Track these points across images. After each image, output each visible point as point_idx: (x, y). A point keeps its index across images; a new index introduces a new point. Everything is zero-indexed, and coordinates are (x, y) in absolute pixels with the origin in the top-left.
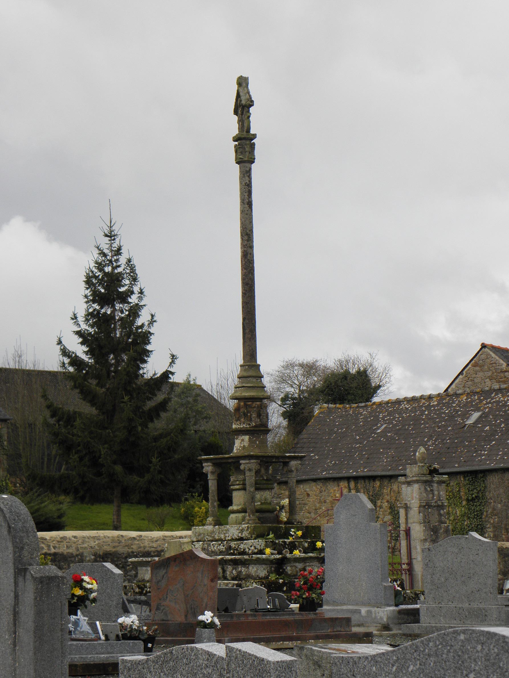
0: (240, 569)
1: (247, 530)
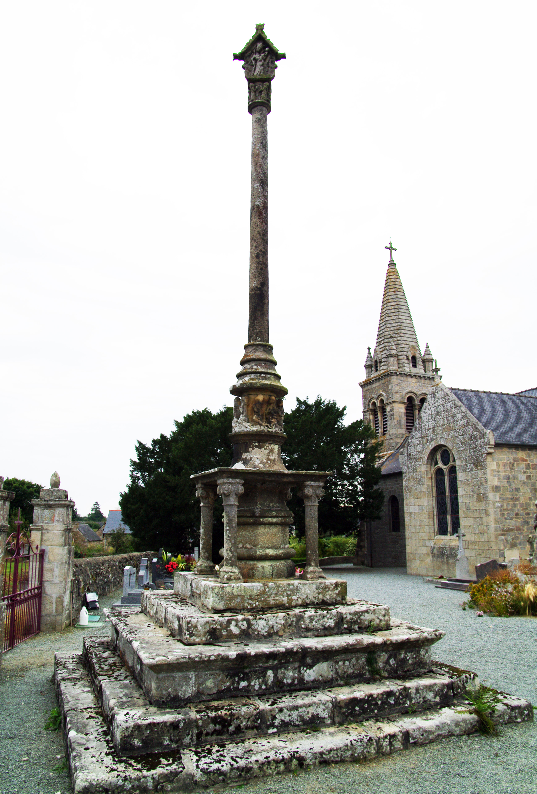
0: (402, 656)
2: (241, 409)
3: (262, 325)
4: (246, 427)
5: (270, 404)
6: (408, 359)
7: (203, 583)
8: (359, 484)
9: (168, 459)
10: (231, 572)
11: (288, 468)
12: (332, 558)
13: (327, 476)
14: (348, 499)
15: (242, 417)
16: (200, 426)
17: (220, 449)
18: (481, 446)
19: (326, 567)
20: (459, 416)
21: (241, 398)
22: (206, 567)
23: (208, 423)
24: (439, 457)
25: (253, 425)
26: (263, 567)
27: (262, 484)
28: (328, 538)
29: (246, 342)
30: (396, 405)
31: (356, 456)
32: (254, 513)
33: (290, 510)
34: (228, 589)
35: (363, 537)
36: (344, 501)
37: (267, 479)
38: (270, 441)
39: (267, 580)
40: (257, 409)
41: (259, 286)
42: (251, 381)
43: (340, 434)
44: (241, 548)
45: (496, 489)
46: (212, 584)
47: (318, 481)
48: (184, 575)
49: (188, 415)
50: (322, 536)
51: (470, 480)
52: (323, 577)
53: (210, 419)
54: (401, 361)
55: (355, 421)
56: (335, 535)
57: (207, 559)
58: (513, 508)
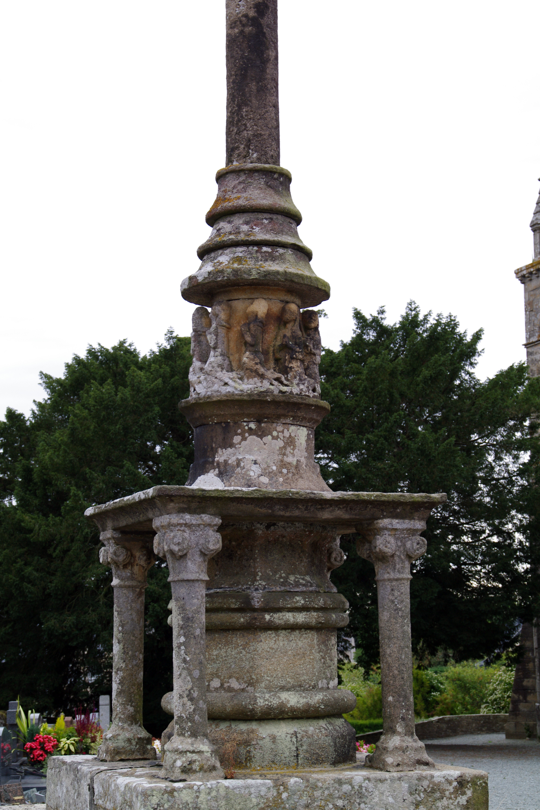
2: (211, 338)
3: (262, 117)
4: (226, 384)
5: (285, 323)
7: (122, 781)
8: (518, 530)
9: (28, 472)
10: (193, 752)
11: (334, 488)
12: (450, 720)
13: (433, 504)
14: (489, 567)
15: (214, 358)
16: (108, 387)
17: (161, 444)
19: (436, 742)
21: (209, 310)
22: (129, 740)
23: (128, 379)
25: (241, 379)
26: (274, 739)
27: (268, 527)
28: (439, 668)
29: (222, 164)
31: (508, 459)
32: (247, 600)
33: (339, 592)
34: (186, 797)
35: (531, 665)
36: (479, 572)
37: (282, 513)
38: (285, 416)
39: (285, 771)
40: (253, 336)
41: (252, 13)
42: (236, 265)
43: (468, 402)
44: (216, 689)
46: (145, 784)
47: (411, 518)
48: (73, 762)
49: (77, 359)
50: (426, 662)
52: (427, 764)
53: (133, 368)
55: (505, 368)
56: (458, 660)
57: (132, 719)
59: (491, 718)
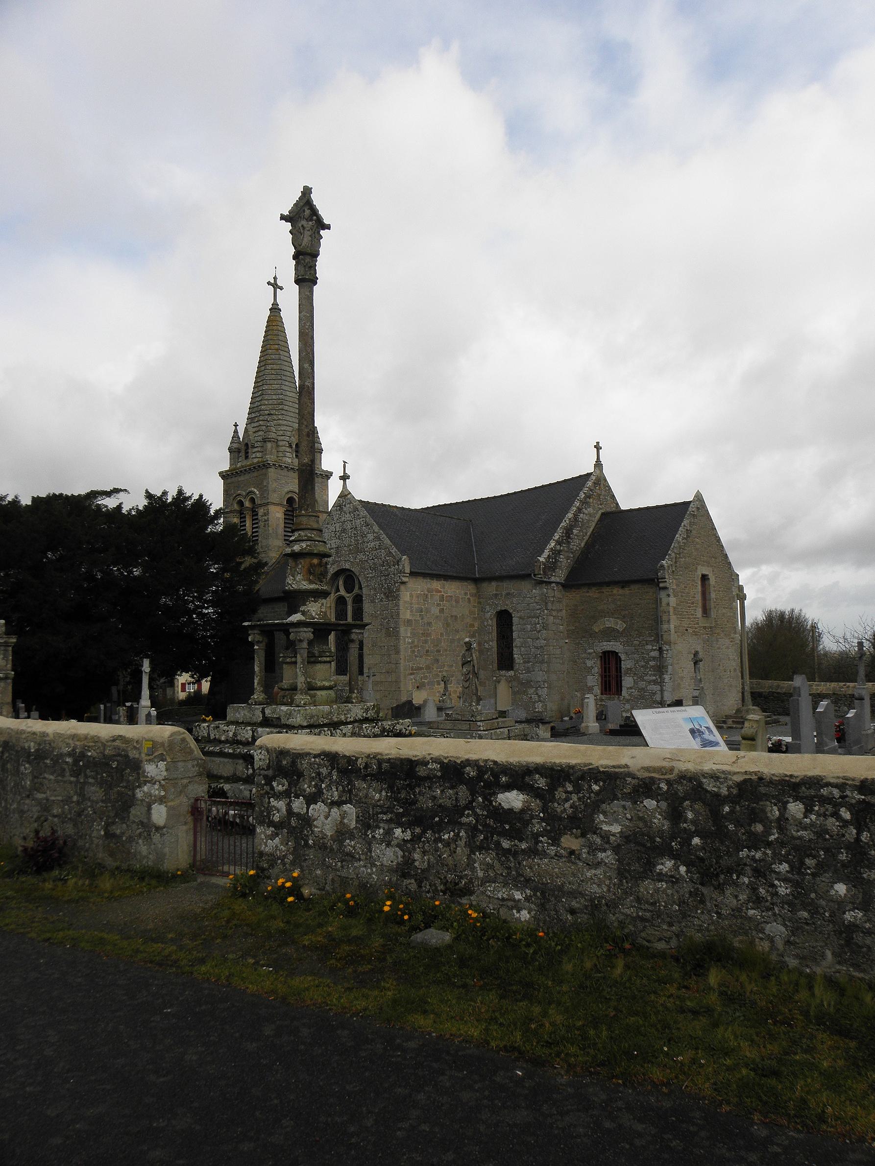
1: (373, 709)
6: (290, 446)
18: (394, 574)
20: (370, 537)
24: (341, 583)
30: (272, 508)
45: (409, 622)
51: (379, 612)
54: (282, 449)
58: (424, 645)
59: (29, 850)
